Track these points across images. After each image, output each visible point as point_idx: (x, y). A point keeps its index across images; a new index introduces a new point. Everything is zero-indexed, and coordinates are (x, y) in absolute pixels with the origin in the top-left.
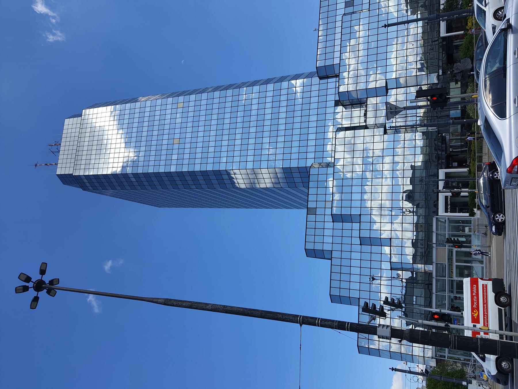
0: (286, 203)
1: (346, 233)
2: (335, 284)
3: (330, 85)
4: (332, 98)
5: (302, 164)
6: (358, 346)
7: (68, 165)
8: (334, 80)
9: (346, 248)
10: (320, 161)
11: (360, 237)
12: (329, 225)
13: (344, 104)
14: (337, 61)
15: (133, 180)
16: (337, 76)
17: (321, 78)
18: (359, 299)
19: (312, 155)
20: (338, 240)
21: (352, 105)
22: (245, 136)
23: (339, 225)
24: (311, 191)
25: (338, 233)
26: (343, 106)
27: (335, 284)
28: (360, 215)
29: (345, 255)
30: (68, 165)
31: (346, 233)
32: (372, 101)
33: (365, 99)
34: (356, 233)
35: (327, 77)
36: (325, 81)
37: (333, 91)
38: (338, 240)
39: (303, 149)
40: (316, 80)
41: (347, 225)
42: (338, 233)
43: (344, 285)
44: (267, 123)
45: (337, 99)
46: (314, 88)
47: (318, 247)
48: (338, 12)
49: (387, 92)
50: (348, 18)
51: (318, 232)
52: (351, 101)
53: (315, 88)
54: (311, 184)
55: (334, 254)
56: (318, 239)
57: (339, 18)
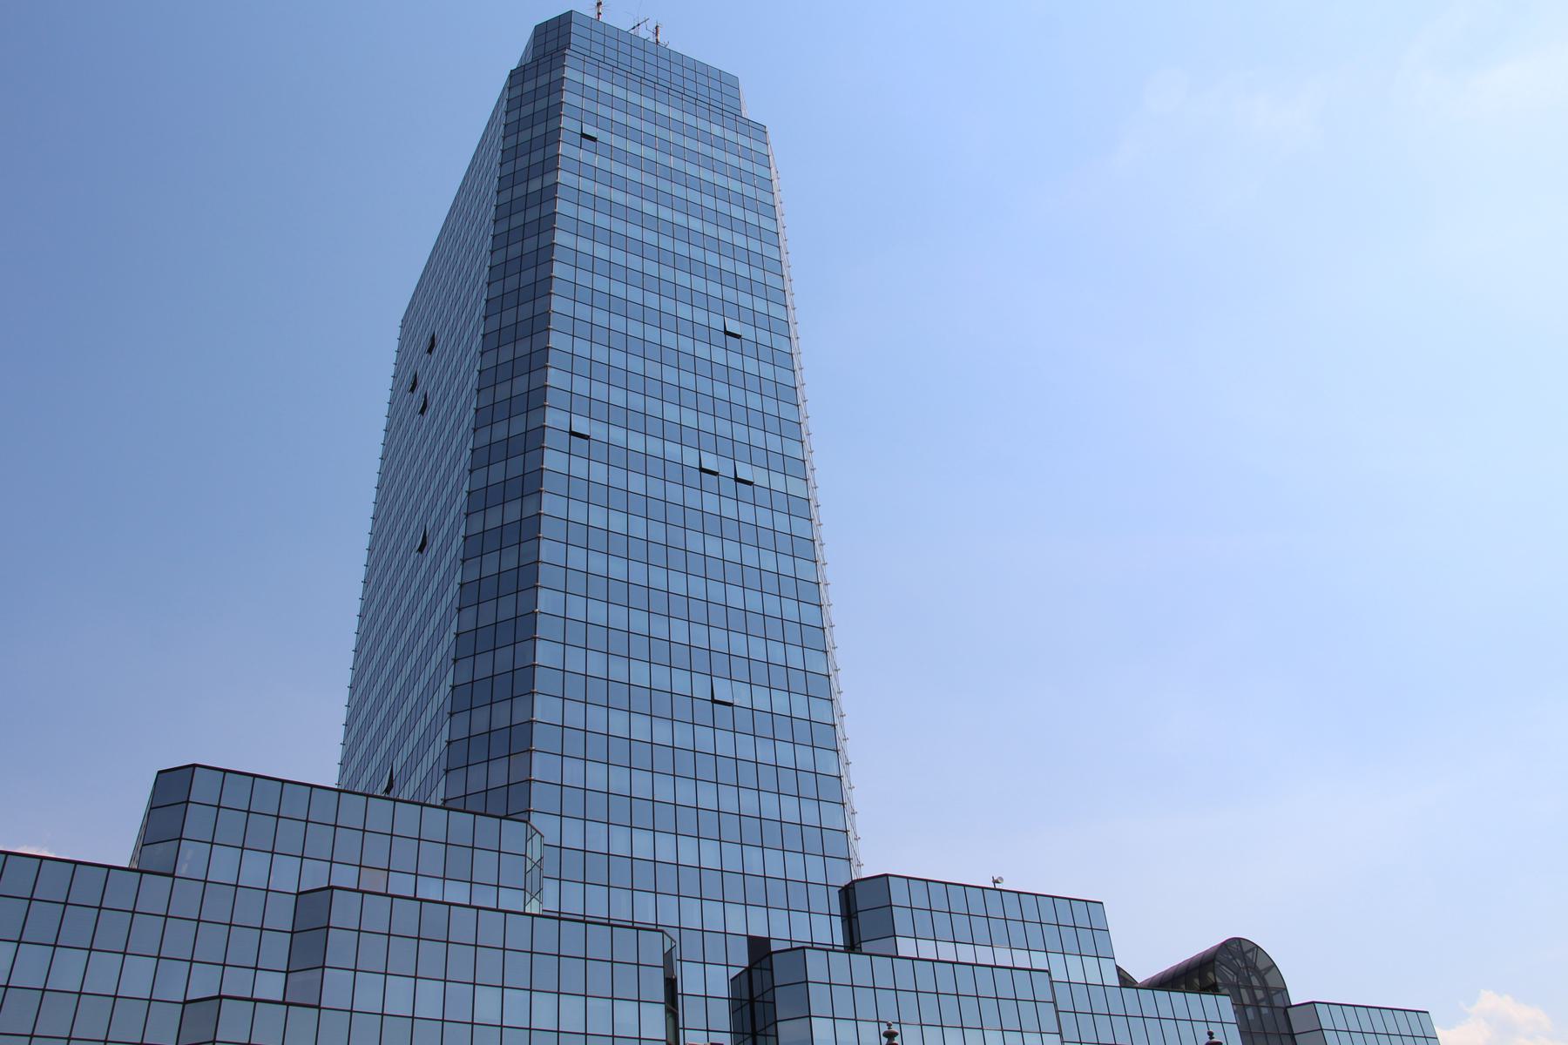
0: (372, 683)
1: (244, 944)
4: (780, 929)
5: (541, 797)
6: (194, 766)
9: (179, 938)
10: (551, 868)
11: (220, 997)
12: (286, 876)
13: (756, 974)
14: (906, 947)
15: (535, 185)
16: (852, 946)
18: (172, 875)
19: (573, 837)
20: (217, 907)
21: (752, 1001)
24: (435, 820)
25: (248, 912)
26: (749, 970)
28: (319, 1007)
29: (146, 933)
31: (244, 944)
34: (237, 983)
37: (802, 936)
39: (597, 806)
41: (277, 950)
42: (248, 912)
45: (775, 946)
47: (340, 944)
52: (768, 997)
54: (462, 821)
56: (373, 950)
57: (1039, 961)
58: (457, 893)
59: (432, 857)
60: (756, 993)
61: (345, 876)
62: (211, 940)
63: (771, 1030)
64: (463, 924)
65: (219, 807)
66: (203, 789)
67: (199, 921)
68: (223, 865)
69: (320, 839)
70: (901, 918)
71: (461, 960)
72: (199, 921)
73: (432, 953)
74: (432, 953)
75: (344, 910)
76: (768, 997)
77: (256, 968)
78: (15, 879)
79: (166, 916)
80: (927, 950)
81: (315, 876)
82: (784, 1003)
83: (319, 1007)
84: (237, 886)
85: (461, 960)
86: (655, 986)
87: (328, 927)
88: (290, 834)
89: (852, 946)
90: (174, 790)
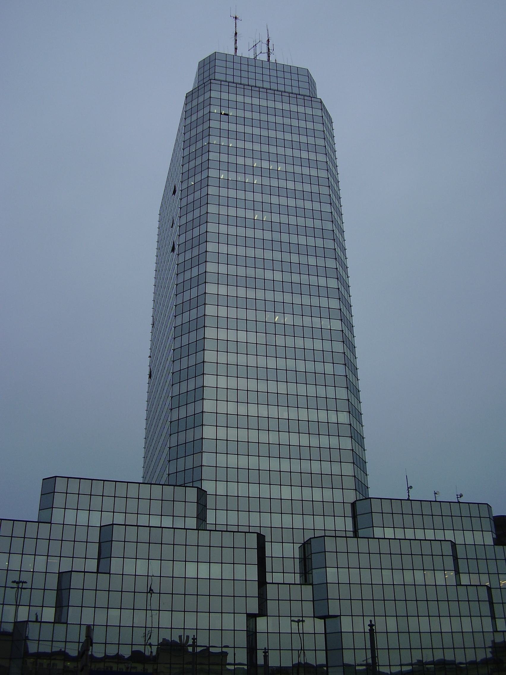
1: (80, 549)
2: (74, 486)
3: (340, 521)
6: (56, 477)
7: (230, 72)
8: (350, 527)
12: (96, 520)
17: (353, 505)
18: (50, 523)
22: (262, 374)
23: (95, 536)
25: (81, 535)
27: (74, 486)
30: (230, 72)
31: (80, 549)
32: (308, 590)
33: (311, 582)
34: (79, 565)
35: (354, 517)
36: (349, 512)
38: (69, 535)
39: (232, 474)
40: (351, 496)
41: (93, 550)
42: (81, 535)
43: (72, 500)
44: (321, 392)
46: (338, 494)
47: (59, 500)
48: (459, 534)
49: (320, 618)
50: (447, 549)
51: (84, 500)
52: (310, 557)
53: (338, 495)
55: (45, 527)
58: (167, 522)
59: (156, 506)
60: (307, 556)
61: (119, 519)
62: (67, 548)
63: (310, 572)
64: (168, 536)
65: (87, 542)
66: (60, 486)
67: (62, 540)
68: (70, 517)
69: (108, 503)
70: (377, 519)
71: (167, 550)
72: (62, 540)
73: (155, 550)
74: (155, 550)
75: (118, 533)
76: (310, 557)
77: (86, 558)
78: (6, 528)
79: (185, 502)
80: (389, 533)
81: (107, 519)
82: (316, 560)
83: (110, 574)
84: (209, 612)
85: (167, 550)
86: (253, 556)
87: (112, 541)
88: (96, 502)
89: (356, 534)
90: (49, 486)
